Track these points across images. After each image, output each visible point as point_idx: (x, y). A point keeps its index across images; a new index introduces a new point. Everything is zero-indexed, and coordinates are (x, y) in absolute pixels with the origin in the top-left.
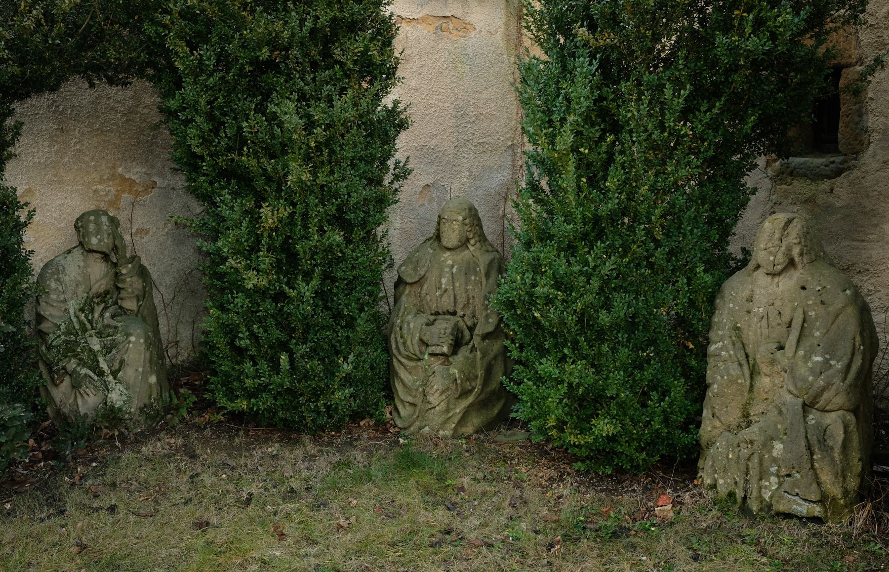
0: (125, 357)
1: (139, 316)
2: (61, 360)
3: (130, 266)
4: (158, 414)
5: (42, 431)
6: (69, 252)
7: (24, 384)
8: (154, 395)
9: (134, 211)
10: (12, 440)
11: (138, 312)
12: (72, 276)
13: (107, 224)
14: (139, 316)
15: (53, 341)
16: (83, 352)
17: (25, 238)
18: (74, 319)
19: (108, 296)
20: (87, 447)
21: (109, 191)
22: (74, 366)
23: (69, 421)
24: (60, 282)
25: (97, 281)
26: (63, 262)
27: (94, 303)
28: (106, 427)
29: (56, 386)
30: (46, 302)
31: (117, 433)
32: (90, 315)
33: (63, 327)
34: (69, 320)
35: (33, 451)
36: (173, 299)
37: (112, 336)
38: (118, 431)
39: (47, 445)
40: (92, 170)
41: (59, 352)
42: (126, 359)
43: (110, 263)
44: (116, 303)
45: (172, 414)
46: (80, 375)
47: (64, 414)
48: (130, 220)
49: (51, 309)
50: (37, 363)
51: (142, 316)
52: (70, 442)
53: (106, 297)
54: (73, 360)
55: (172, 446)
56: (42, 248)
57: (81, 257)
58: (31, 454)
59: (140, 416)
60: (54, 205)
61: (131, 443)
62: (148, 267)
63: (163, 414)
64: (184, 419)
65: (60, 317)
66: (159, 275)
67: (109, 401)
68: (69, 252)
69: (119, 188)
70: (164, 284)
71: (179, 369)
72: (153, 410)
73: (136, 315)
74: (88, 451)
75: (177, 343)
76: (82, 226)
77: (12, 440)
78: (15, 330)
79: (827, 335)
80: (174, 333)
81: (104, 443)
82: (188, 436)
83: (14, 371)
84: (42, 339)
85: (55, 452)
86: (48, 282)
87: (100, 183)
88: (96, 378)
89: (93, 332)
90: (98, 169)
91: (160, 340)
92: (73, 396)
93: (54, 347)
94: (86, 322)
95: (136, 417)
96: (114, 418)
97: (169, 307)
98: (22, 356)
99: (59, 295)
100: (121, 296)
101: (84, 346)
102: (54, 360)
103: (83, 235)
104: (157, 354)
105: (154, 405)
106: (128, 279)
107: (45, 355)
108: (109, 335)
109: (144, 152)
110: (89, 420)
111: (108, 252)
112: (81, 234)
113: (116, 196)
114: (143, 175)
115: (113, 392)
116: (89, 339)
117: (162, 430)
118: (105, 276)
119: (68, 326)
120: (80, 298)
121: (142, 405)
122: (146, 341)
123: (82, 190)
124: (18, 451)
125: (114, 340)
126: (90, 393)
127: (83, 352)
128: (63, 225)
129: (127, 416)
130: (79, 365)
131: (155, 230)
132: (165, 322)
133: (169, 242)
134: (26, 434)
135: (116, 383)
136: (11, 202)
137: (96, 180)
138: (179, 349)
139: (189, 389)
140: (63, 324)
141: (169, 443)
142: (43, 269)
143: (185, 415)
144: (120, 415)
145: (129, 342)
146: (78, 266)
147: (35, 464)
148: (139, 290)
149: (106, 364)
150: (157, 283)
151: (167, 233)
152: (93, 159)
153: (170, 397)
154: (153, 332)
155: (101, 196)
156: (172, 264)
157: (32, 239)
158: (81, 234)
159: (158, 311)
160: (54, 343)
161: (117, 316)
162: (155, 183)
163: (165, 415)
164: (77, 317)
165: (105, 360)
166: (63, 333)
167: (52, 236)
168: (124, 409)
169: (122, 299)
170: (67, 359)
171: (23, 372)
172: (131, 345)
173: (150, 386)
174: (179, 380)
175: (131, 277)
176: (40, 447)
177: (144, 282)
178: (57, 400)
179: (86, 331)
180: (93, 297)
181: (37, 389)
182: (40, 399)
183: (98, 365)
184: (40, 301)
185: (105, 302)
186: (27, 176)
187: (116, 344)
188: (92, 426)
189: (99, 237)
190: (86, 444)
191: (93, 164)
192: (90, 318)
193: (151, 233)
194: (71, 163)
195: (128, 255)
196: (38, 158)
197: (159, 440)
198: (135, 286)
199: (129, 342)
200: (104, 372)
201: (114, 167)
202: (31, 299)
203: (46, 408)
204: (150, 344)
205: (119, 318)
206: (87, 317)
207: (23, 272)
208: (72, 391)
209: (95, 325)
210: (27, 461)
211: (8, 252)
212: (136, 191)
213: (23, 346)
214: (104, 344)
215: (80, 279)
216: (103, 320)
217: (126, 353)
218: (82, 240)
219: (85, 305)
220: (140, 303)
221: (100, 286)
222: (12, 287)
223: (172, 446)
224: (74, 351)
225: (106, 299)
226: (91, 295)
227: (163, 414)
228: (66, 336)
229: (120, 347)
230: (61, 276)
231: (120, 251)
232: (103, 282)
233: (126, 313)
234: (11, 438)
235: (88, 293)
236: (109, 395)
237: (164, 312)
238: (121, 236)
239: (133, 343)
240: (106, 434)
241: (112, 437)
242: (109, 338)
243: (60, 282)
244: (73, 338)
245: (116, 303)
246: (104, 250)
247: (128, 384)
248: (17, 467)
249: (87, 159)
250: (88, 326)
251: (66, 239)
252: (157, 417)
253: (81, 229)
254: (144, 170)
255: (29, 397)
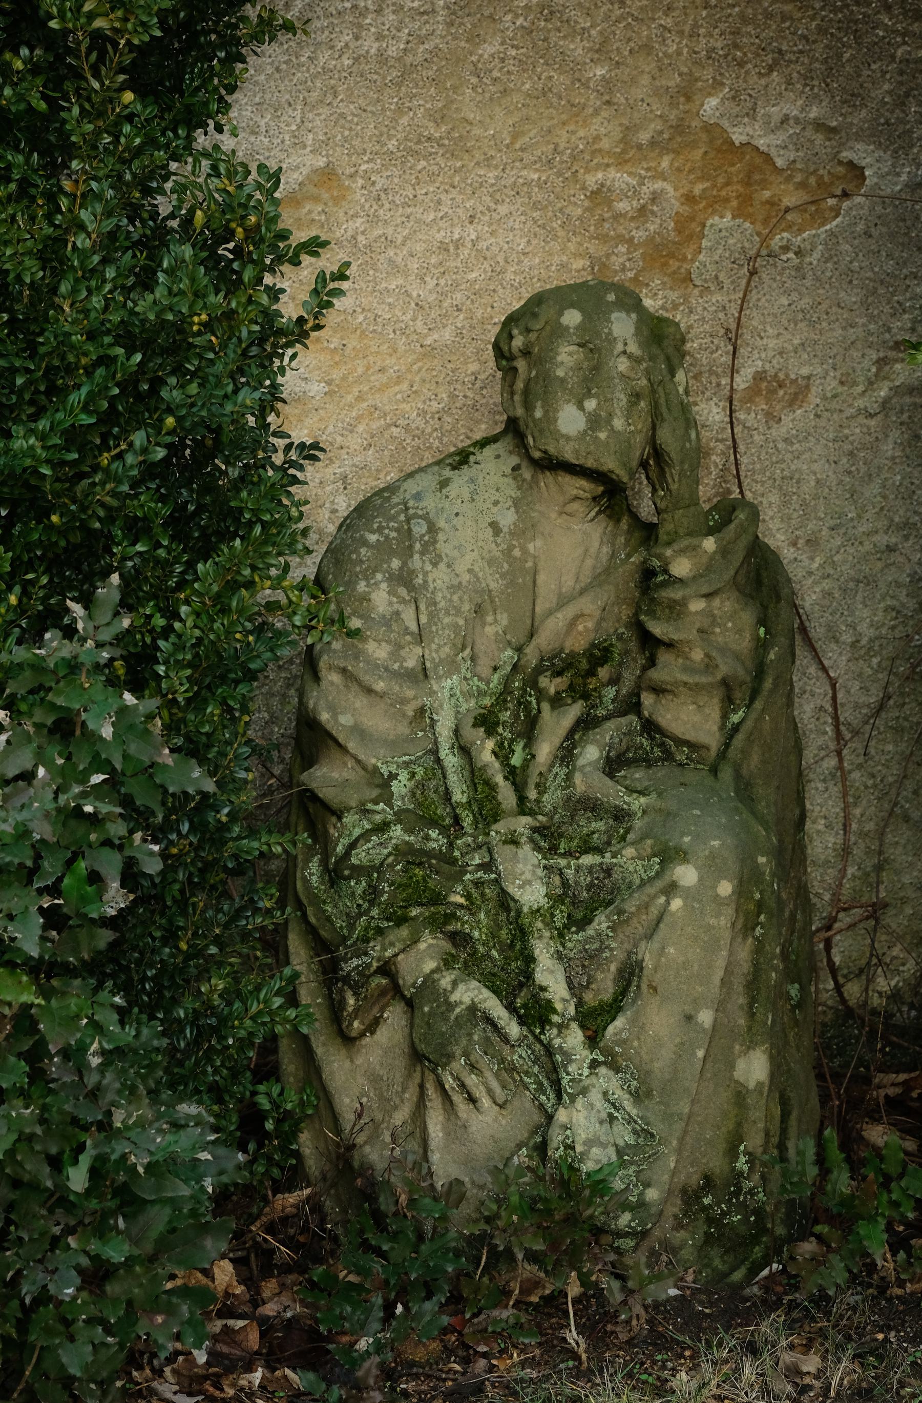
0: (648, 955)
1: (727, 774)
2: (380, 931)
3: (709, 544)
4: (761, 1228)
5: (270, 1229)
6: (462, 459)
7: (224, 1021)
8: (754, 1141)
9: (753, 296)
10: (152, 1259)
11: (722, 755)
12: (462, 567)
13: (633, 348)
14: (727, 774)
15: (353, 846)
16: (471, 908)
17: (289, 382)
18: (451, 760)
19: (603, 673)
20: (445, 1331)
21: (655, 198)
22: (430, 965)
23: (385, 1204)
24: (410, 586)
25: (563, 601)
26: (430, 503)
27: (541, 694)
28: (532, 1257)
29: (348, 1040)
30: (344, 671)
31: (574, 1290)
32: (518, 748)
33: (401, 787)
34: (430, 761)
35: (227, 1312)
36: (881, 707)
37: (599, 851)
38: (584, 1280)
39: (285, 1299)
40: (594, 101)
41: (373, 893)
42: (649, 963)
43: (624, 524)
44: (632, 705)
45: (819, 1238)
46: (451, 1006)
47: (366, 1168)
48: (734, 338)
49: (360, 702)
50: (281, 930)
51: (738, 776)
52: (379, 1301)
53: (592, 673)
54: (428, 941)
55: (806, 1389)
56: (351, 428)
57: (510, 490)
58: (217, 1326)
59: (679, 1226)
60: (419, 247)
61: (630, 1342)
62: (787, 554)
63: (780, 1231)
64: (871, 1267)
65: (393, 745)
66: (828, 594)
67: (556, 1138)
68: (462, 459)
69: (698, 189)
70: (847, 638)
71: (873, 1033)
72: (742, 1207)
73: (714, 771)
74: (449, 1351)
75: (876, 911)
76: (526, 353)
77: (152, 1259)
78: (210, 786)
79: (727, 392)
80: (869, 864)
81: (518, 1326)
82: (880, 1351)
83: (188, 957)
84: (313, 835)
85: (313, 1334)
86: (362, 587)
87: (621, 162)
88: (514, 1030)
89: (523, 824)
90: (619, 98)
91: (802, 893)
92: (411, 1094)
93: (358, 871)
94: (499, 779)
95: (664, 1230)
96: (571, 1220)
97: (858, 744)
98: (225, 894)
99: (399, 647)
100: (656, 675)
101: (478, 884)
102: (352, 927)
103: (526, 392)
104: (784, 956)
105: (747, 1185)
106: (697, 606)
107: (316, 900)
108: (587, 848)
109: (821, 31)
110: (466, 1209)
111: (622, 474)
112: (520, 385)
113: (681, 223)
114: (809, 133)
115: (580, 1102)
116: (503, 854)
117: (770, 1306)
118: (601, 578)
119: (421, 785)
120: (484, 669)
121: (696, 1180)
122: (741, 892)
123: (541, 185)
124: (170, 1311)
125: (608, 872)
126: (480, 1092)
127: (471, 908)
128: (447, 335)
129: (624, 1219)
130: (448, 962)
131: (832, 384)
132: (834, 808)
133: (888, 448)
134: (209, 1243)
135: (594, 1064)
136: (252, 234)
137: (605, 144)
138: (882, 937)
139: (906, 1131)
140: (403, 776)
141: (794, 1372)
142: (347, 525)
143: (880, 1253)
144: (596, 1211)
145: (672, 889)
146: (494, 525)
147: (229, 1370)
148: (737, 656)
149: (561, 976)
150: (817, 631)
151: (885, 404)
152: (601, 51)
153: (821, 1159)
154: (778, 854)
155: (618, 217)
156: (890, 549)
157: (316, 389)
158: (520, 385)
159: (809, 755)
160: (360, 857)
161: (629, 763)
162: (856, 171)
163: (792, 1240)
164: (465, 751)
165: (560, 956)
166: (400, 816)
167: (399, 380)
168: (618, 1185)
169: (658, 690)
170: (404, 932)
171: (220, 965)
172: (676, 904)
173: (740, 1096)
174: (867, 1080)
175: (708, 596)
176: (256, 1301)
177: (762, 621)
178: (346, 1105)
179: (496, 816)
180: (539, 670)
181: (271, 1044)
182: (276, 1090)
183: (529, 975)
184: (322, 665)
185: (585, 696)
186: (325, 111)
187: (615, 890)
188: (477, 1241)
189: (591, 404)
190: (445, 1320)
191: (600, 71)
192: (516, 760)
193: (814, 398)
194: (511, 66)
195: (707, 491)
196: (379, 37)
197: (753, 1350)
198: (720, 636)
199: (672, 889)
200: (549, 1007)
201: (687, 93)
202: (285, 652)
203: (293, 1135)
204: (760, 906)
205: (639, 775)
206: (502, 753)
207: (267, 539)
208: (409, 1076)
209: (532, 794)
210: (201, 1357)
211: (217, 441)
212: (771, 203)
213: (235, 857)
214: (565, 884)
215: (495, 584)
216: (569, 777)
217: (649, 937)
218: (520, 412)
219: (501, 700)
220: (735, 718)
221: (572, 624)
222: (217, 598)
223: (806, 1389)
224: (437, 899)
225: (592, 683)
226: (531, 657)
227: (780, 1231)
228: (409, 831)
229: (631, 906)
230: (416, 562)
231: (673, 473)
232: (589, 605)
233: (668, 756)
234: (148, 1247)
235: (519, 650)
236: (562, 1116)
237: (833, 762)
238: (685, 409)
239: (687, 893)
240: (530, 1286)
241: (555, 1301)
242: (588, 860)
243: (410, 586)
244: (436, 840)
245: (632, 705)
246: (610, 463)
247: (644, 1076)
248: (158, 1373)
249: (577, 48)
250: (507, 795)
251: (453, 397)
252: (754, 1240)
253: (521, 364)
254: (814, 112)
255: (235, 1075)
